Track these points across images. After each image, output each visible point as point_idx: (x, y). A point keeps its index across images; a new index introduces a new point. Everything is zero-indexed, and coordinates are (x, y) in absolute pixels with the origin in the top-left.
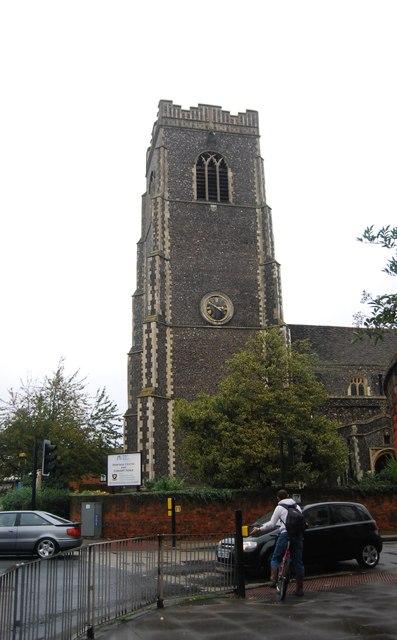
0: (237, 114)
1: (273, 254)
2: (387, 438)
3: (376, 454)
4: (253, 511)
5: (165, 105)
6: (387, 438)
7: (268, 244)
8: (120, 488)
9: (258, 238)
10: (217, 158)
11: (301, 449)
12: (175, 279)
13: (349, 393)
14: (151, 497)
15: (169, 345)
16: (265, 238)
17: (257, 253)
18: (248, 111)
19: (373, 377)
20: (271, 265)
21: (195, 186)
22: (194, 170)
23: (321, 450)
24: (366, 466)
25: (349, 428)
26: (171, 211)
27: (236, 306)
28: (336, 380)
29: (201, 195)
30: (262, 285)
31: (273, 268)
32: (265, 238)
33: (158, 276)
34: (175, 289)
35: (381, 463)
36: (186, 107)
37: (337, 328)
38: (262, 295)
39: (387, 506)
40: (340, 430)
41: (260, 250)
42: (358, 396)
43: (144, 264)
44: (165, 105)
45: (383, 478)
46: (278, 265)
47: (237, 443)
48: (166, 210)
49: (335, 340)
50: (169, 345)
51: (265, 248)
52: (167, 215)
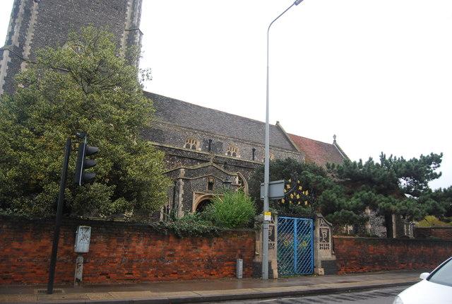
1: (138, 24)
2: (211, 185)
3: (199, 198)
4: (16, 245)
6: (211, 185)
7: (136, 14)
9: (128, 8)
11: (104, 166)
12: (41, 20)
14: (308, 218)
16: (133, 8)
17: (124, 20)
20: (134, 31)
23: (133, 172)
24: (188, 203)
25: (177, 171)
28: (174, 138)
31: (136, 34)
32: (133, 8)
33: (22, 10)
34: (38, 29)
35: (201, 206)
37: (182, 102)
40: (169, 174)
41: (128, 18)
42: (191, 150)
45: (204, 218)
46: (141, 34)
47: (16, 148)
49: (179, 110)
51: (132, 17)
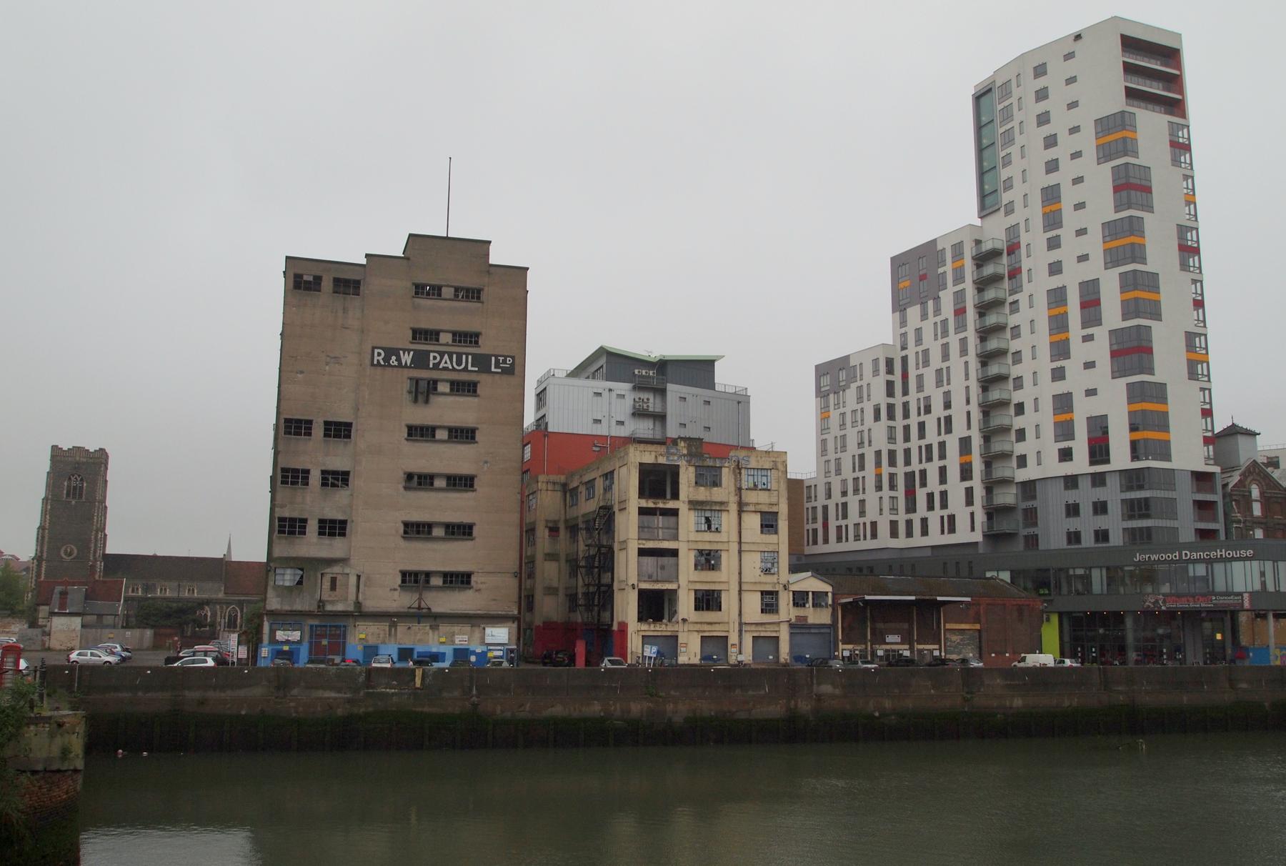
0: (66, 449)
5: (54, 448)
8: (509, 639)
10: (79, 476)
13: (159, 593)
15: (43, 569)
18: (74, 447)
19: (144, 584)
21: (65, 492)
22: (66, 484)
26: (51, 505)
27: (78, 551)
29: (68, 495)
30: (93, 541)
36: (65, 448)
38: (93, 545)
39: (1284, 652)
41: (95, 523)
43: (1232, 597)
44: (54, 448)
48: (49, 504)
50: (43, 569)
52: (49, 507)
